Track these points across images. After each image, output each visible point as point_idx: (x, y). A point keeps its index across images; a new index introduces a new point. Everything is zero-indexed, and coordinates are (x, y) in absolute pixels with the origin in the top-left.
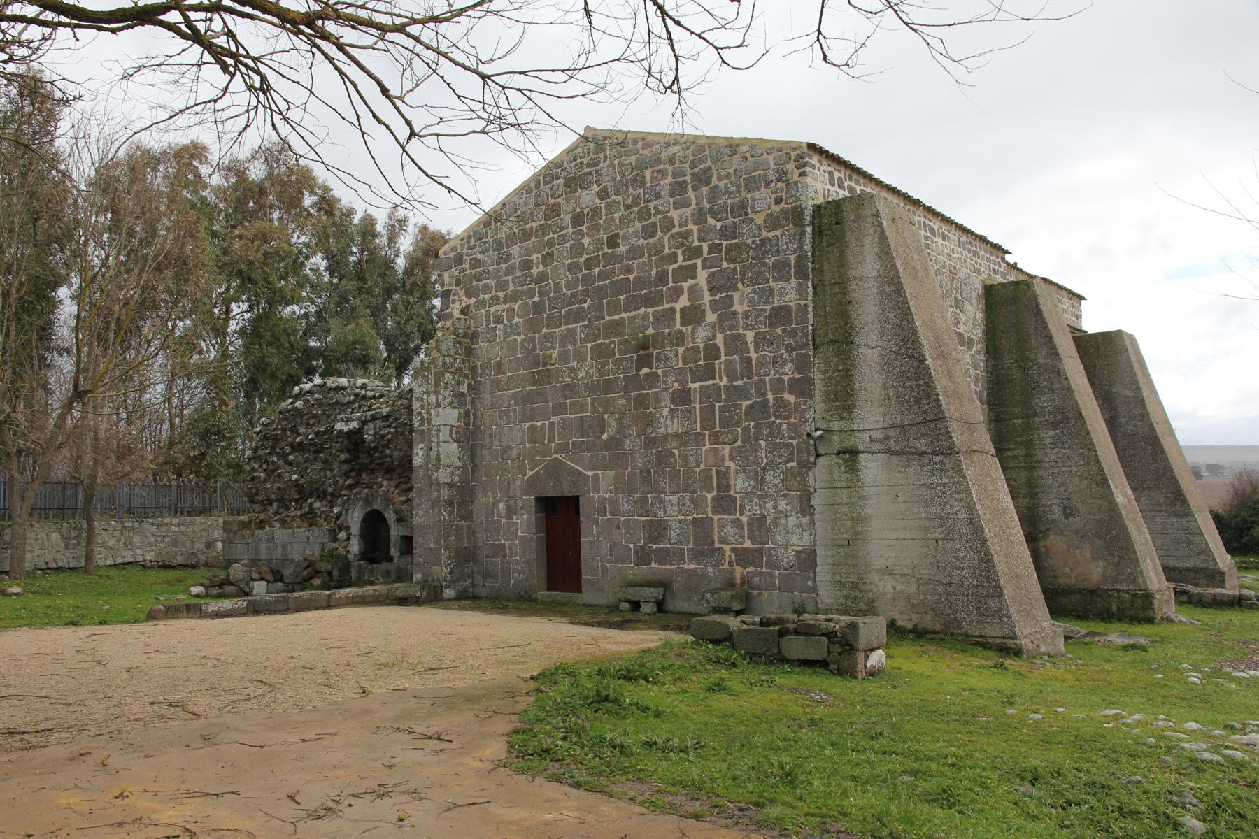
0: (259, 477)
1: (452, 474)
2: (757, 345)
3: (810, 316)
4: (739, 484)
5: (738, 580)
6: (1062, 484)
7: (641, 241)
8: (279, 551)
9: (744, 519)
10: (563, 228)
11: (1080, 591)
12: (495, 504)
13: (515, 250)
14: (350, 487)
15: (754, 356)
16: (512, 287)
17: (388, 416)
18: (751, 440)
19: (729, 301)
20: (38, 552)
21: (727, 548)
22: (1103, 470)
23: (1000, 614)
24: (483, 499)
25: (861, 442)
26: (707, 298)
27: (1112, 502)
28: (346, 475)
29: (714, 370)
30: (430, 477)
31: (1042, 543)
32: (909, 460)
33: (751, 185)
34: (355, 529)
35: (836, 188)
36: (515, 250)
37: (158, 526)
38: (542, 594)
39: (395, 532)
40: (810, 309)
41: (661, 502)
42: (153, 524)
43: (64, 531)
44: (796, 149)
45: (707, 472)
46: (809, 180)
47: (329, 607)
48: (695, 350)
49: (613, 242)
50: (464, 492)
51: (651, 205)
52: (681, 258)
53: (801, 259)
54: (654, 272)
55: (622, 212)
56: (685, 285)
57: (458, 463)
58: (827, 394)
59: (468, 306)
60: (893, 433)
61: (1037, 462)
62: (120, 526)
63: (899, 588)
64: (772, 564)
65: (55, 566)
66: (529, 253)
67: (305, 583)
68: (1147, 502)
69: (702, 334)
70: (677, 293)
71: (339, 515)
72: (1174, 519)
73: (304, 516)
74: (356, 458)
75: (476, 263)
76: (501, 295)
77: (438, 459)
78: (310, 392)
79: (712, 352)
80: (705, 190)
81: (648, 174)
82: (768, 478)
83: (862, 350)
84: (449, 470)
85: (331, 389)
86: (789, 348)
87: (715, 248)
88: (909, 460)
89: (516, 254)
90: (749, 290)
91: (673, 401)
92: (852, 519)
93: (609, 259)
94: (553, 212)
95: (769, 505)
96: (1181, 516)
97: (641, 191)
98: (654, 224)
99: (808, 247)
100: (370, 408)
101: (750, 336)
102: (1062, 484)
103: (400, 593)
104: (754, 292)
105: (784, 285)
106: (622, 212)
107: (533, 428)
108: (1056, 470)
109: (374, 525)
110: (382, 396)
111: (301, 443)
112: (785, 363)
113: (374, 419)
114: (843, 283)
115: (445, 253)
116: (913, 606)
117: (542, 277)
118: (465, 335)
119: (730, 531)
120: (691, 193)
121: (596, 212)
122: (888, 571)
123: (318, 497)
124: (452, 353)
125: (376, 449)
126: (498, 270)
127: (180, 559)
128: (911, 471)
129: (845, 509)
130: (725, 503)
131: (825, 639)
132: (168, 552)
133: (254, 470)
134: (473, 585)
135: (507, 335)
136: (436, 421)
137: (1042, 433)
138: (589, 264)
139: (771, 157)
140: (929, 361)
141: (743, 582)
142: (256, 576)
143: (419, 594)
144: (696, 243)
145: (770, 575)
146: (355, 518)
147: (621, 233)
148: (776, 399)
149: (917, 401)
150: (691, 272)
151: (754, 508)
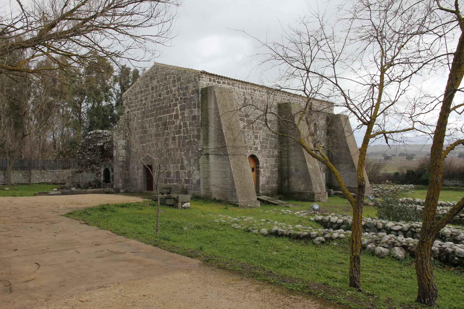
0: (80, 158)
1: (123, 158)
2: (189, 125)
3: (200, 118)
4: (186, 162)
5: (185, 188)
6: (295, 162)
7: (166, 96)
8: (85, 179)
9: (186, 171)
10: (149, 91)
11: (298, 193)
12: (134, 167)
13: (139, 96)
14: (102, 161)
15: (189, 128)
16: (138, 107)
17: (110, 142)
18: (188, 150)
19: (184, 113)
20: (15, 179)
21: (183, 179)
22: (305, 158)
23: (235, 196)
24: (132, 165)
25: (210, 152)
26: (179, 112)
27: (307, 168)
28: (101, 158)
29: (180, 132)
30: (117, 159)
31: (290, 179)
32: (219, 157)
33: (189, 82)
34: (102, 174)
35: (212, 82)
36: (139, 96)
37: (52, 172)
38: (145, 191)
39: (111, 174)
40: (200, 116)
41: (169, 167)
42: (51, 172)
43: (23, 173)
44: (198, 73)
45: (179, 158)
46: (201, 81)
47: (85, 194)
48: (177, 126)
49: (160, 96)
50: (127, 164)
51: (168, 86)
52: (174, 101)
53: (198, 103)
54: (168, 104)
55: (162, 87)
56: (175, 108)
57: (125, 155)
58: (203, 139)
59: (128, 111)
60: (216, 149)
61: (290, 156)
62: (40, 172)
63: (216, 190)
64: (192, 184)
65: (21, 183)
66: (142, 97)
67: (87, 188)
68: (345, 167)
69: (178, 122)
70: (173, 110)
71: (99, 169)
72: (352, 173)
73: (91, 169)
74: (103, 153)
75: (131, 99)
76: (136, 108)
77: (119, 154)
78: (93, 134)
79: (180, 127)
80: (179, 82)
81: (168, 77)
82: (191, 161)
83: (211, 127)
84: (122, 157)
85: (97, 133)
86: (196, 126)
87: (181, 99)
88: (219, 157)
89: (139, 97)
90: (188, 110)
91: (172, 140)
92: (208, 172)
93: (159, 100)
94: (147, 86)
95: (191, 168)
96: (353, 172)
97: (166, 82)
98: (169, 91)
99: (200, 100)
100: (106, 139)
101: (188, 123)
102: (295, 162)
103: (107, 191)
104: (189, 111)
105: (195, 109)
106: (162, 87)
107: (143, 146)
108: (294, 158)
109: (107, 172)
110: (110, 136)
111: (90, 148)
112: (195, 131)
113: (107, 142)
114: (207, 109)
115: (124, 96)
116: (219, 194)
117: (145, 104)
118: (128, 120)
119: (184, 174)
120: (177, 83)
121: (156, 87)
122: (214, 185)
123: (95, 164)
124: (123, 125)
125: (107, 151)
126: (136, 101)
127: (59, 182)
128: (219, 159)
129: (206, 169)
130: (182, 168)
131: (173, 200)
132: (55, 180)
133: (79, 156)
134: (130, 189)
135: (137, 120)
136: (119, 144)
137: (291, 147)
138: (155, 101)
139: (193, 75)
140: (224, 131)
141: (186, 188)
142: (72, 186)
143: (113, 191)
144: (177, 97)
145: (191, 186)
146: (102, 170)
147: (162, 93)
148: (193, 140)
149: (221, 141)
150: (175, 105)
151: (188, 169)
